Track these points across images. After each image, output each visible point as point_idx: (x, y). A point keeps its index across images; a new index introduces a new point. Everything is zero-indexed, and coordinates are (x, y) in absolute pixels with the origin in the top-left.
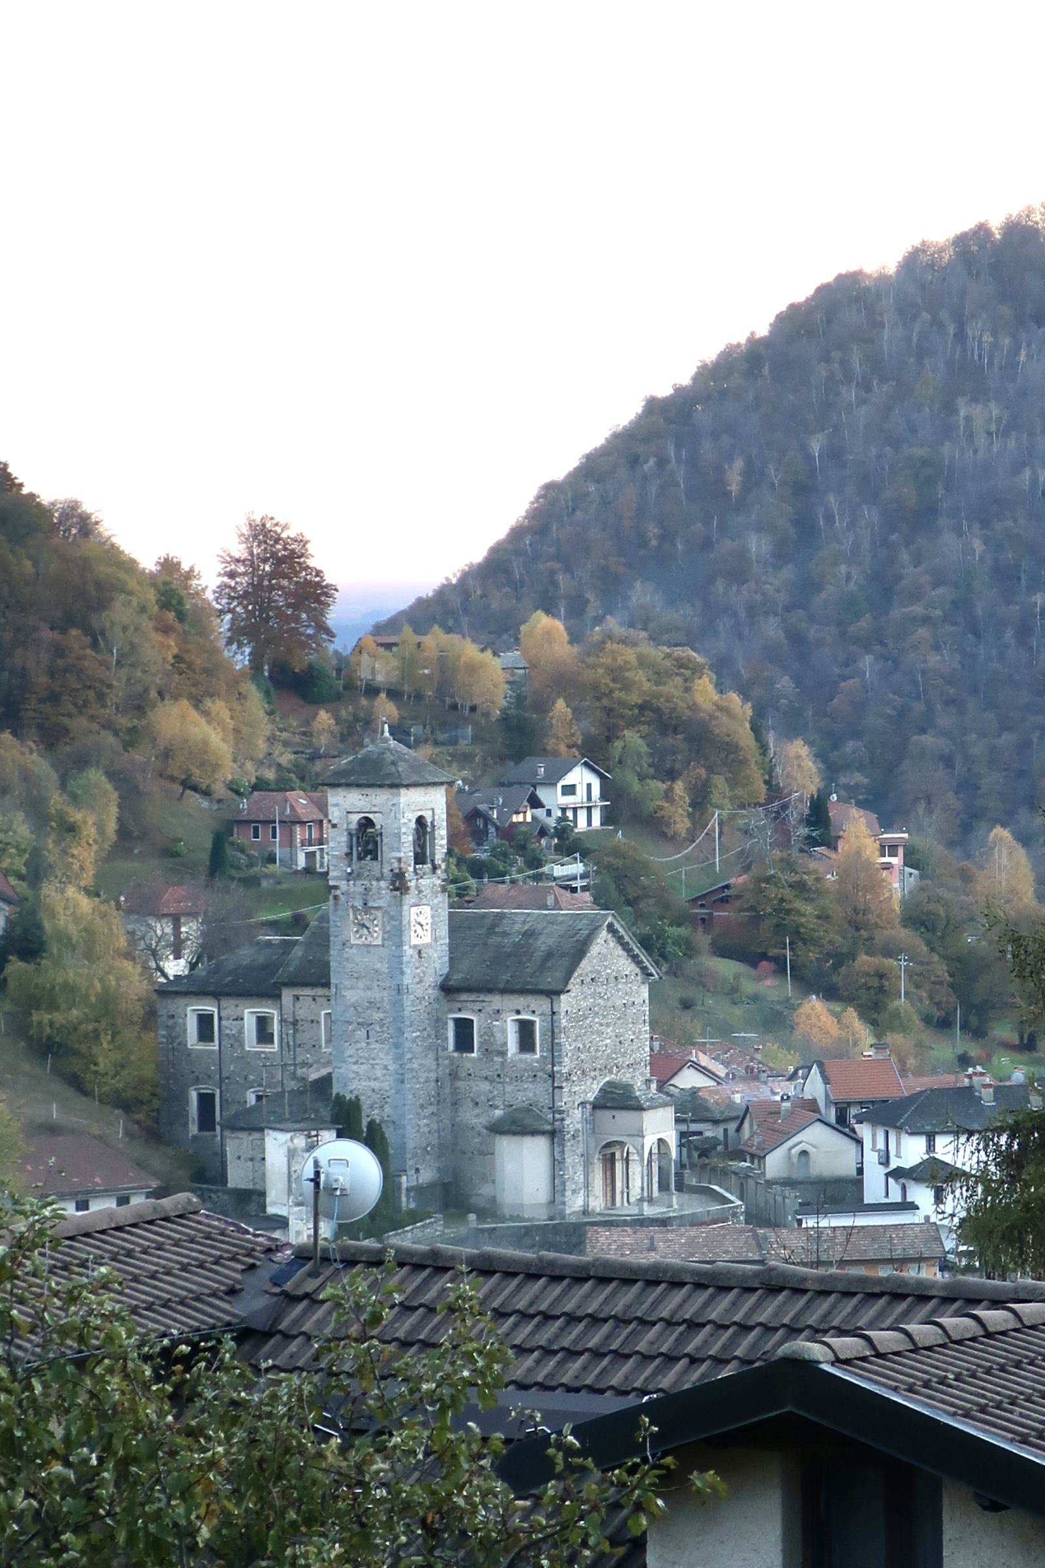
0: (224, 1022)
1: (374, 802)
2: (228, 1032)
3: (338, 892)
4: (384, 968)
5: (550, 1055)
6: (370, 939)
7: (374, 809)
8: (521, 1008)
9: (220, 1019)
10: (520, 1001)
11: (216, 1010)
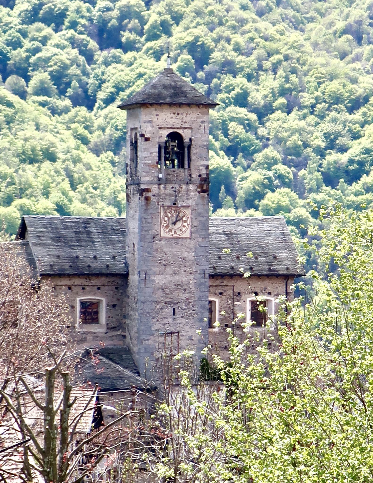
3: (149, 194)
8: (258, 291)
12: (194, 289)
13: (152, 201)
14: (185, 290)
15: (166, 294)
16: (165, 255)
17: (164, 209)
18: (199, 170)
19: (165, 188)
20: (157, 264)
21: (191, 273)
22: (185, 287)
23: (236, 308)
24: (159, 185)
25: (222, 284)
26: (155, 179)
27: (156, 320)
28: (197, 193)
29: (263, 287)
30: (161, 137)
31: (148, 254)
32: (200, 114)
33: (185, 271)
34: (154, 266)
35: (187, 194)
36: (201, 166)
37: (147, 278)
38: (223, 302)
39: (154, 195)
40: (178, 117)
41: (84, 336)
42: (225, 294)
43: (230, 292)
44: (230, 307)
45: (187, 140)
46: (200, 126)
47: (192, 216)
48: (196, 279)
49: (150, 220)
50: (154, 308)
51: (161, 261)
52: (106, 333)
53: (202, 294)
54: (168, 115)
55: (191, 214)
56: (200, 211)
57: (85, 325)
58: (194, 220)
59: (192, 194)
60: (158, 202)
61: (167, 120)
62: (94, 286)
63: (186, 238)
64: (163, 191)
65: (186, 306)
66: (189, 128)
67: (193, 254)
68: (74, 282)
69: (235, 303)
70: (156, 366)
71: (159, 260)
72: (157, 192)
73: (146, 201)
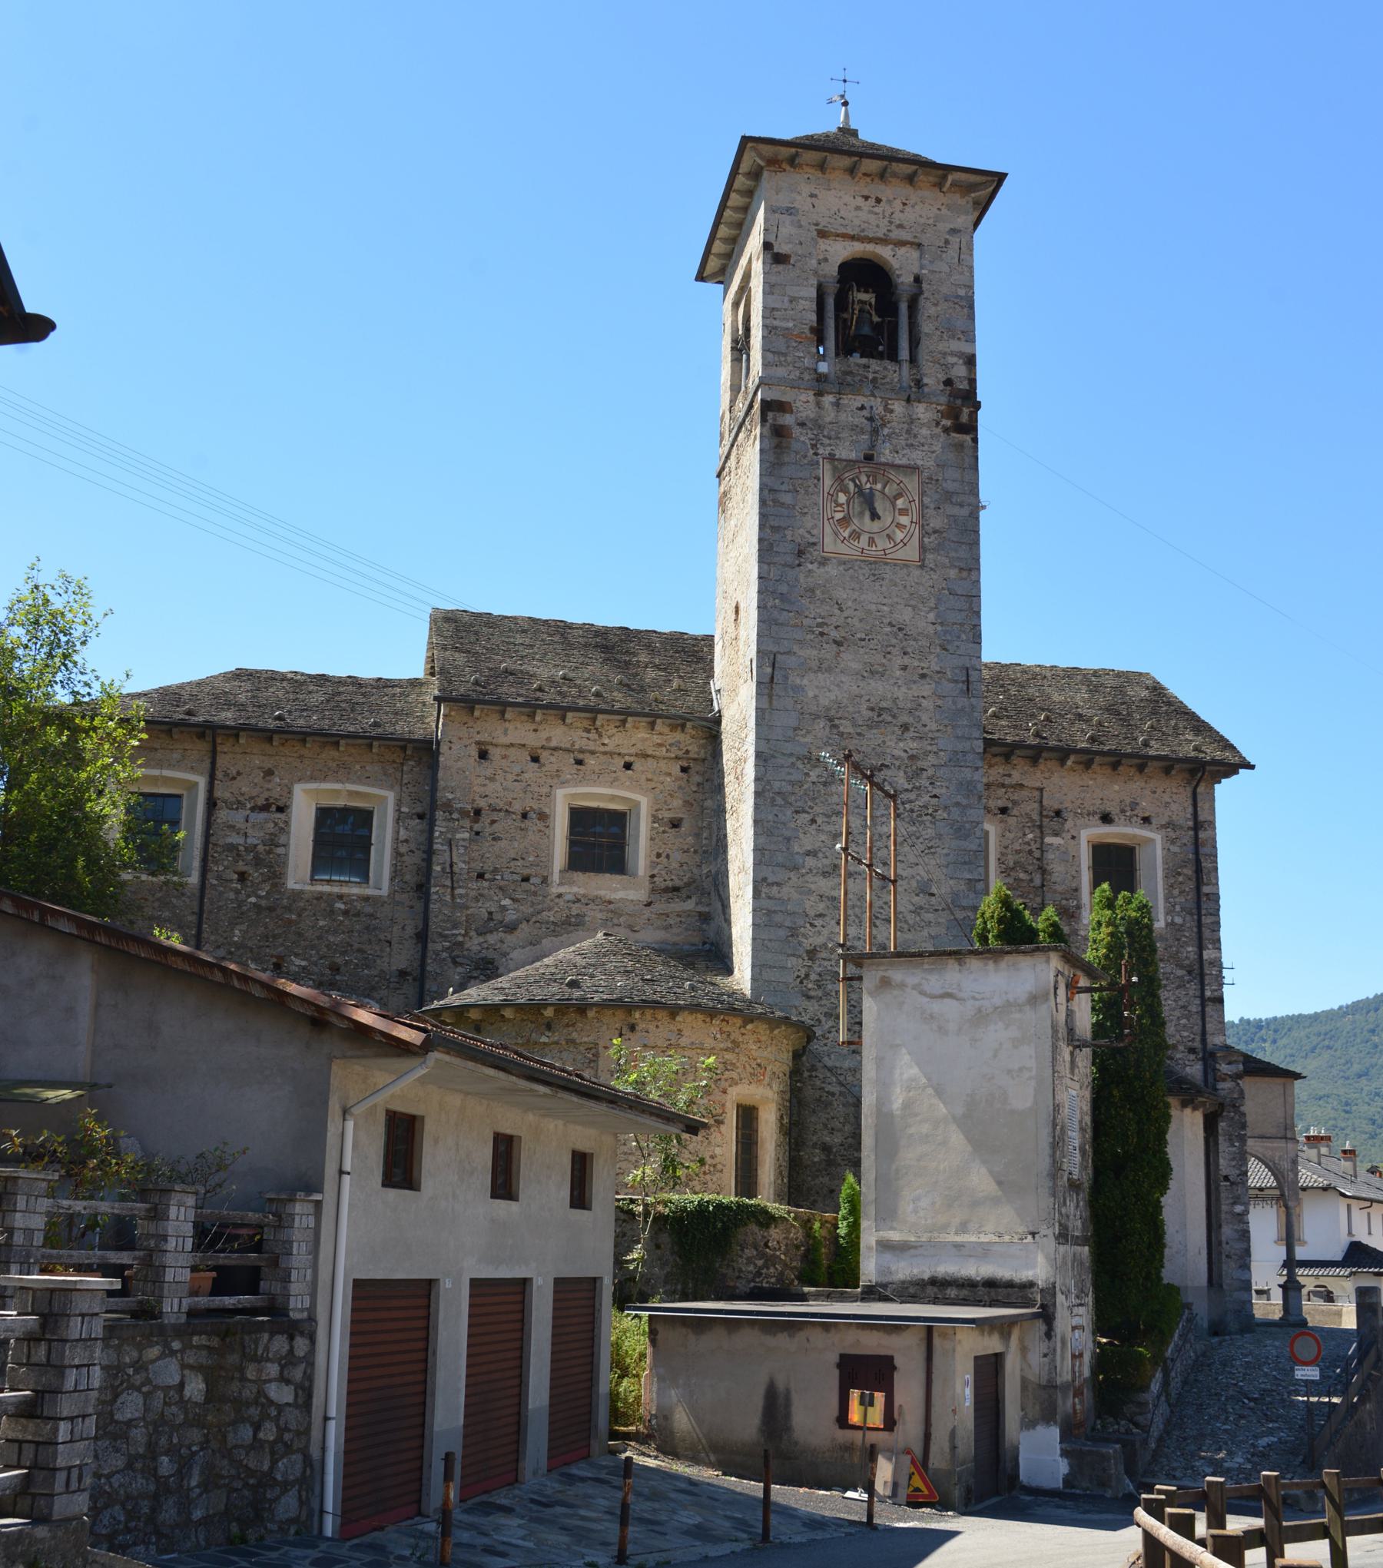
0: (222, 815)
1: (898, 218)
2: (235, 839)
3: (788, 420)
4: (924, 622)
5: (1191, 923)
6: (882, 543)
7: (897, 234)
8: (1113, 809)
9: (212, 804)
10: (1112, 790)
11: (202, 782)
12: (934, 726)
13: (797, 440)
14: (905, 727)
15: (841, 734)
16: (837, 612)
17: (835, 469)
18: (947, 367)
19: (837, 404)
20: (810, 636)
21: (923, 676)
22: (904, 718)
23: (1050, 856)
24: (819, 394)
25: (1007, 781)
26: (806, 377)
27: (808, 817)
28: (938, 430)
29: (1128, 801)
30: (826, 260)
31: (782, 600)
32: (944, 211)
33: (904, 668)
34: (801, 642)
35: (908, 432)
36: (952, 354)
37: (778, 678)
38: (1012, 836)
39: (802, 424)
40: (876, 210)
41: (575, 909)
42: (1015, 812)
43: (1031, 808)
44: (1030, 852)
45: (905, 279)
46: (947, 242)
47: (927, 500)
48: (940, 697)
49: (787, 499)
50: (800, 777)
51: (825, 630)
52: (649, 904)
53: (960, 747)
54: (847, 199)
55: (923, 493)
56: (950, 486)
57: (579, 877)
58: (931, 512)
59: (925, 432)
60: (814, 446)
61: (842, 214)
62: (611, 754)
63: (905, 565)
64: (830, 415)
65: (909, 780)
66: (912, 244)
67: (931, 616)
68: (549, 739)
69: (1048, 840)
70: (807, 976)
71: (819, 625)
72: (812, 416)
73: (776, 440)
